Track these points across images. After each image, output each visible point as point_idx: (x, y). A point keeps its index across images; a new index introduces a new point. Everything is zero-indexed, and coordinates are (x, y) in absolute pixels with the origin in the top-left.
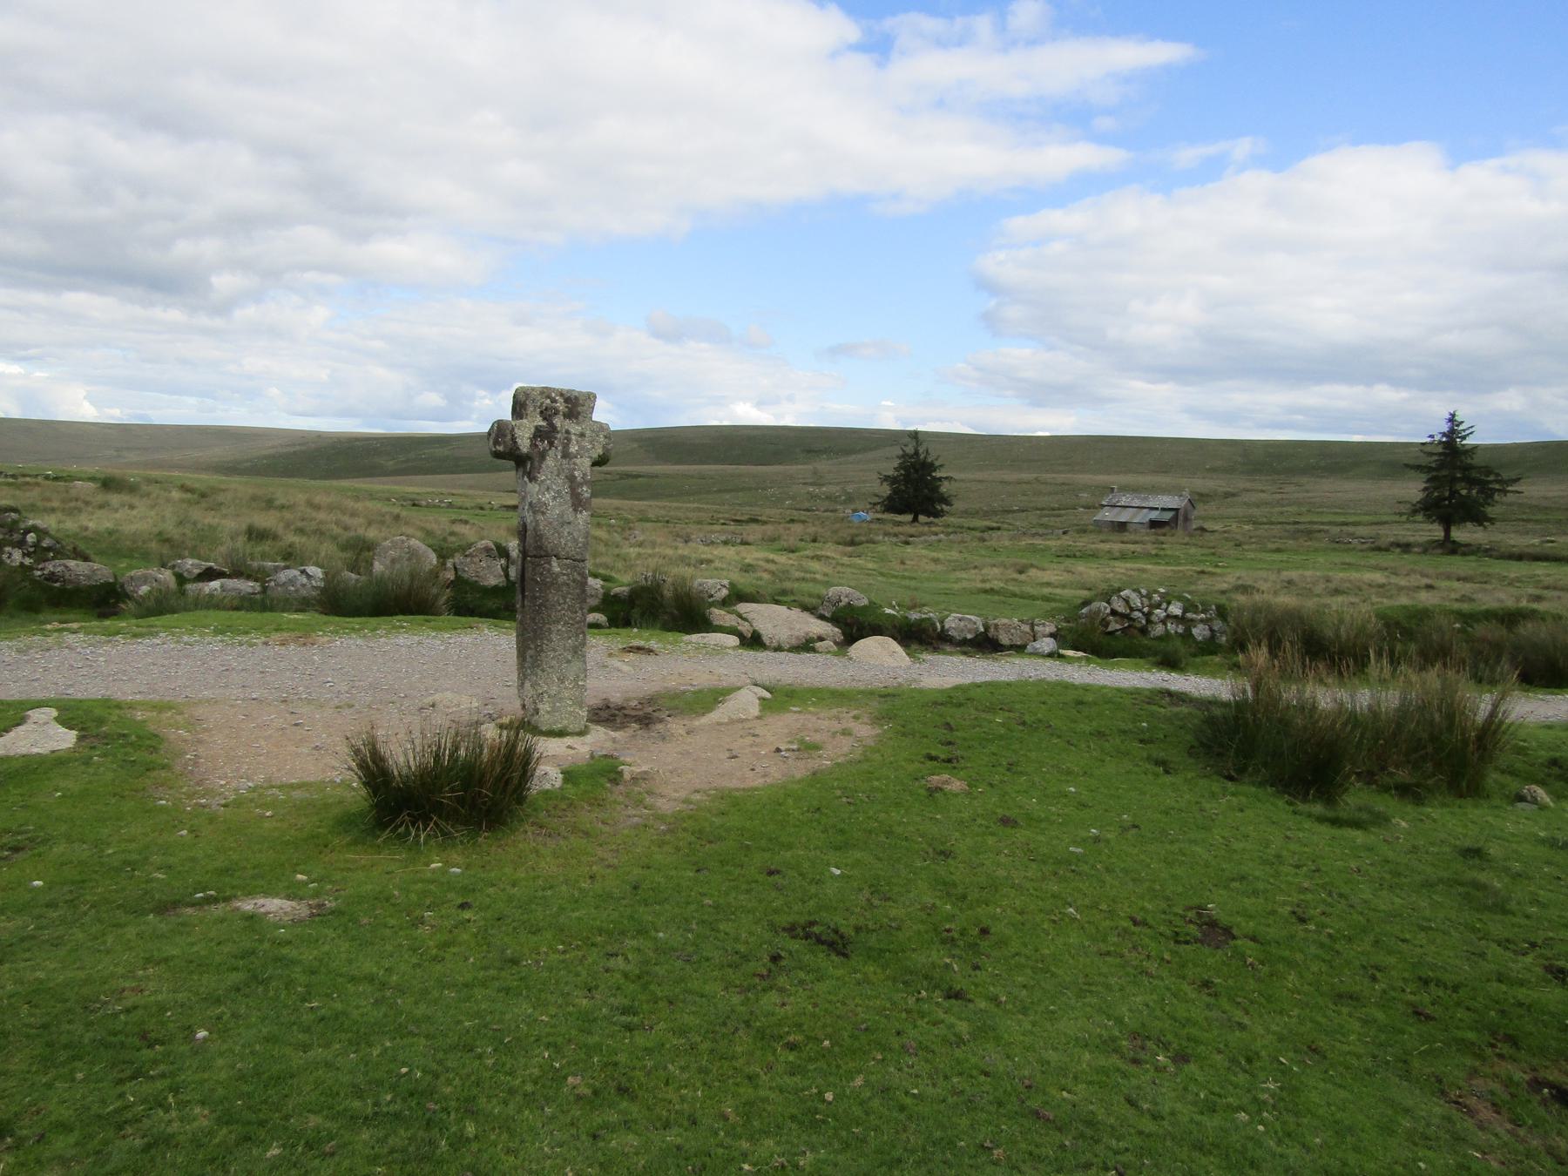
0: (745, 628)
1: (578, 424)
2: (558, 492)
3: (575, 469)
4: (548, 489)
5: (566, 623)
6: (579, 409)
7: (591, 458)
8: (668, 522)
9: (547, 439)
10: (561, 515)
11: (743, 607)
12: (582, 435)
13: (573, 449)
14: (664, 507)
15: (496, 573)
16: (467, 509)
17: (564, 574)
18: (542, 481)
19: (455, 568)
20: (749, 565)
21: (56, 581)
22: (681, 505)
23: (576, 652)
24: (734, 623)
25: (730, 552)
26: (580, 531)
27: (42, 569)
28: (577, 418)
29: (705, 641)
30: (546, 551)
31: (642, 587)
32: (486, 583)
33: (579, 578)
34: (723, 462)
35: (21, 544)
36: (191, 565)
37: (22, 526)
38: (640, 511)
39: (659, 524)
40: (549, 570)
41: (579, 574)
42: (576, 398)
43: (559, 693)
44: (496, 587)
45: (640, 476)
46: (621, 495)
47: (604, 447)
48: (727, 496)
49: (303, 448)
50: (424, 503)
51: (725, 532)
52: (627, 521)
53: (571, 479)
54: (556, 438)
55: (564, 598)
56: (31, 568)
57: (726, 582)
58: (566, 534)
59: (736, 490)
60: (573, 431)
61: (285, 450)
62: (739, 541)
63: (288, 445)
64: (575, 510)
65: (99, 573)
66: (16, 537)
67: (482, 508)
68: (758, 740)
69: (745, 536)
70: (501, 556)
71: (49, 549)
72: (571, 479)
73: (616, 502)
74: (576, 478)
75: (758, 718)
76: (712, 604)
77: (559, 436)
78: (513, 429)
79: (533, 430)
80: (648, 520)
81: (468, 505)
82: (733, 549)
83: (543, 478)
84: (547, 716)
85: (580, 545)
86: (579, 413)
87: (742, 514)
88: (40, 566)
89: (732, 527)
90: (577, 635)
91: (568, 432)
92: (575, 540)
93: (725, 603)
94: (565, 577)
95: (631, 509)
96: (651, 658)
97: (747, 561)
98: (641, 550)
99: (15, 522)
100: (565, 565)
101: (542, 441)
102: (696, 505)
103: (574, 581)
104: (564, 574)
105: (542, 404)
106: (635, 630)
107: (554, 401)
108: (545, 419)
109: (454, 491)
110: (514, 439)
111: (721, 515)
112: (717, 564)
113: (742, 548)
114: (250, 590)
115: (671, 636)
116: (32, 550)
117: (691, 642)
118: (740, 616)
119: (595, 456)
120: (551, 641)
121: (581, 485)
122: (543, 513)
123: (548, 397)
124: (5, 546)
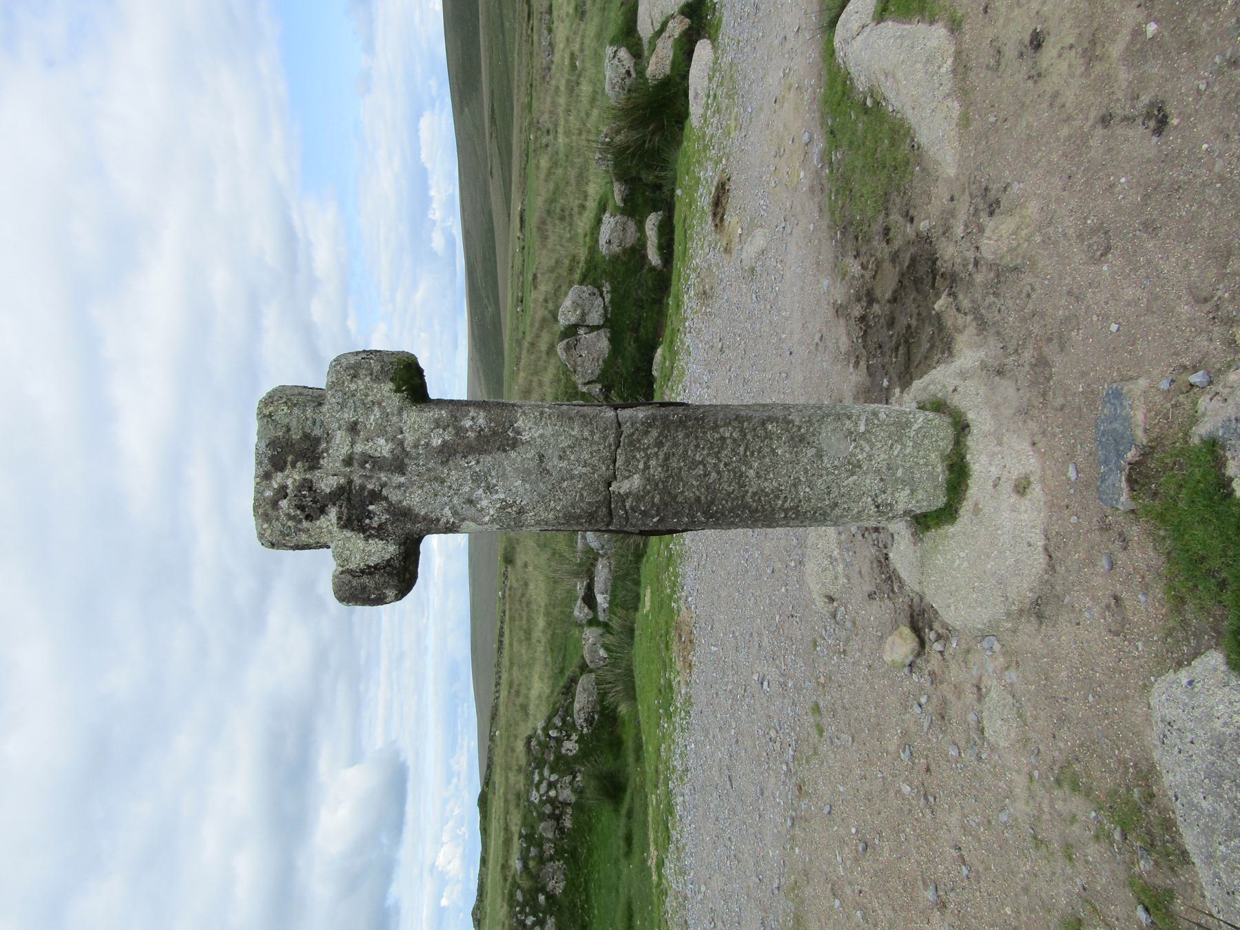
0: (677, 28)
1: (329, 437)
2: (476, 479)
3: (427, 444)
4: (470, 502)
5: (744, 461)
6: (296, 436)
7: (401, 410)
8: (531, 85)
9: (364, 505)
10: (525, 475)
11: (645, 28)
12: (353, 428)
13: (383, 448)
14: (518, 87)
15: (595, 340)
16: (524, 261)
17: (647, 467)
18: (455, 513)
19: (589, 383)
20: (576, 9)
21: (593, 717)
22: (516, 69)
23: (802, 439)
24: (670, 43)
25: (562, 31)
26: (556, 435)
27: (582, 727)
28: (317, 440)
29: (702, 94)
30: (599, 505)
31: (615, 166)
32: (607, 351)
33: (655, 433)
34: (476, 27)
35: (559, 741)
36: (580, 612)
37: (542, 738)
38: (522, 110)
39: (534, 94)
40: (639, 499)
41: (646, 433)
42: (272, 444)
43: (878, 471)
44: (610, 340)
45: (493, 106)
46: (508, 125)
47: (377, 379)
48: (507, 24)
49: (481, 371)
50: (520, 294)
51: (539, 31)
52: (531, 123)
53: (447, 453)
54: (363, 487)
55: (694, 464)
56: (581, 736)
57: (610, 50)
58: (564, 464)
59: (501, 16)
60: (345, 450)
61: (483, 381)
62: (548, 17)
63: (480, 381)
64: (514, 444)
65: (586, 686)
66: (552, 743)
67: (523, 248)
68: (1063, 35)
69: (543, 10)
70: (576, 334)
71: (564, 721)
72: (447, 453)
73: (516, 130)
74: (445, 443)
75: (955, 26)
76: (641, 73)
77: (357, 481)
78: (350, 572)
79: (348, 533)
80: (530, 105)
81: (521, 259)
82: (556, 23)
83: (447, 512)
84: (920, 495)
85: (586, 434)
86: (306, 436)
87: (523, 11)
88: (580, 729)
89: (535, 23)
90: (769, 436)
91: (348, 461)
92: (576, 444)
93: (637, 54)
94: (653, 463)
95: (521, 118)
96: (731, 186)
97: (571, 11)
98: (560, 130)
99: (539, 743)
100: (627, 462)
101: (370, 515)
102: (516, 56)
103: (660, 444)
104: (647, 467)
105: (290, 517)
106: (679, 192)
107: (282, 492)
108: (322, 511)
109: (510, 265)
110: (370, 571)
111: (524, 32)
112: (577, 47)
113: (555, 13)
114: (606, 570)
115: (690, 145)
116: (564, 733)
117: (704, 116)
118: (659, 33)
119: (396, 400)
120: (777, 492)
121: (460, 431)
122: (521, 511)
123: (275, 504)
124: (560, 752)
